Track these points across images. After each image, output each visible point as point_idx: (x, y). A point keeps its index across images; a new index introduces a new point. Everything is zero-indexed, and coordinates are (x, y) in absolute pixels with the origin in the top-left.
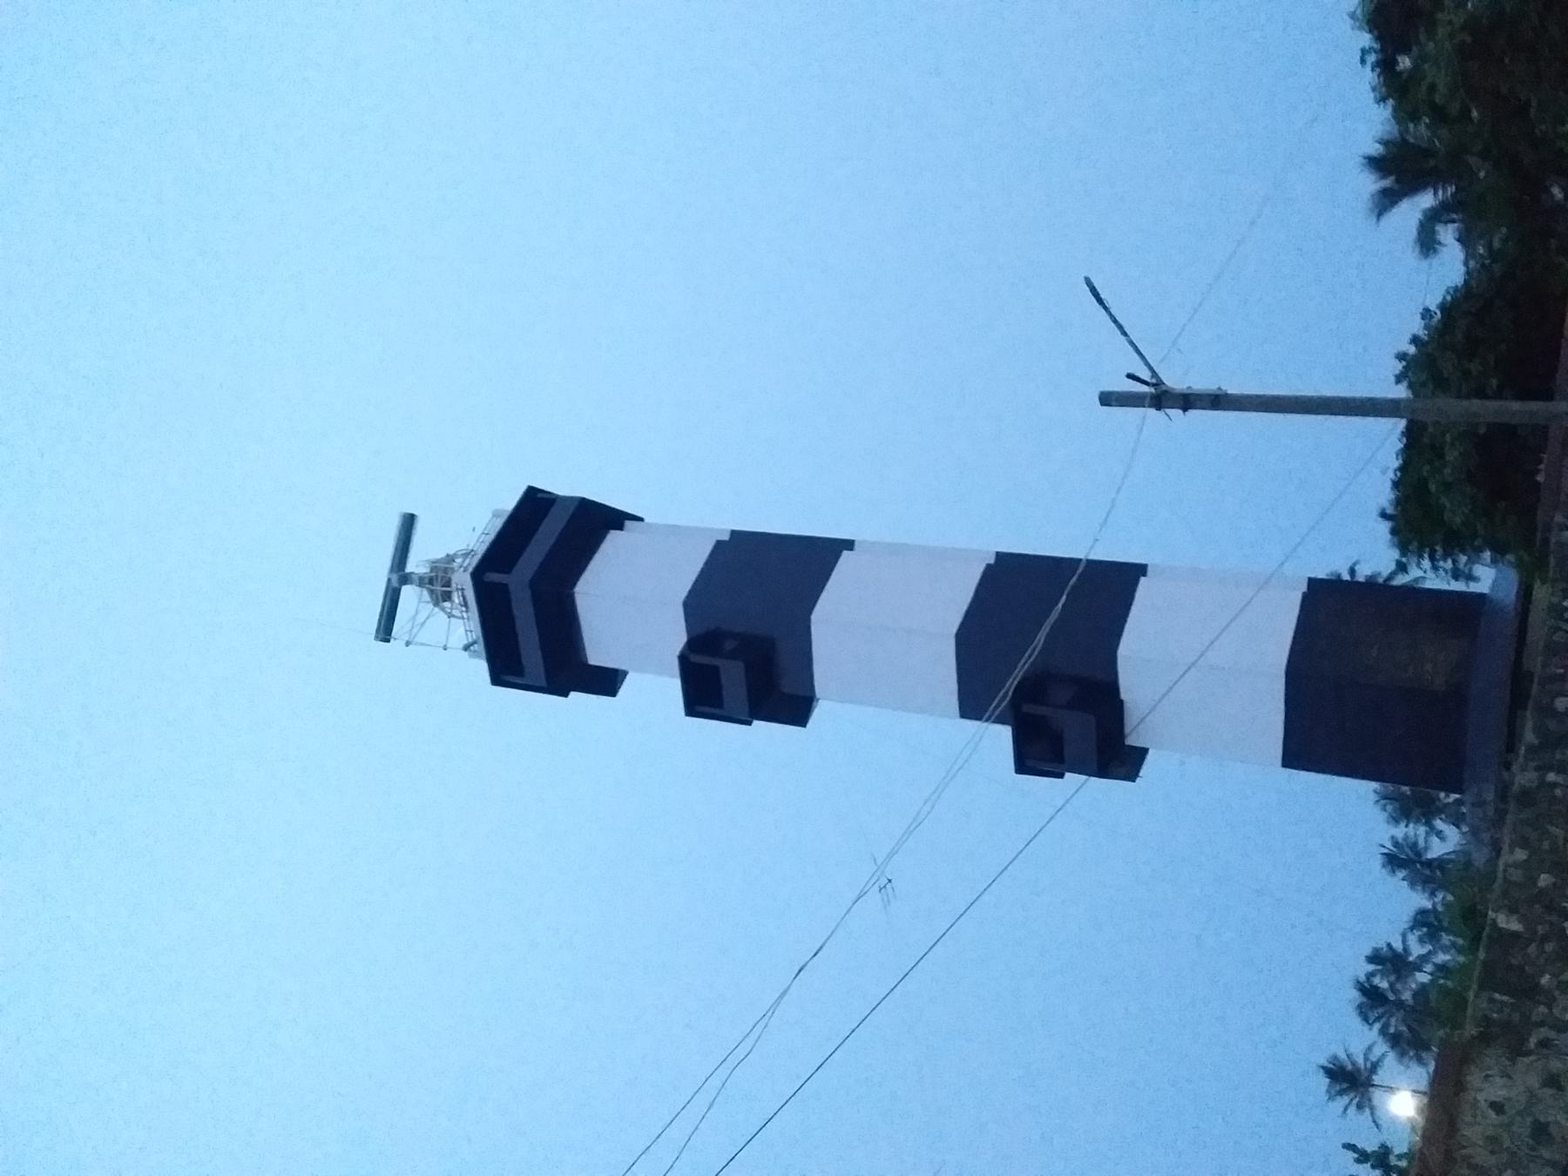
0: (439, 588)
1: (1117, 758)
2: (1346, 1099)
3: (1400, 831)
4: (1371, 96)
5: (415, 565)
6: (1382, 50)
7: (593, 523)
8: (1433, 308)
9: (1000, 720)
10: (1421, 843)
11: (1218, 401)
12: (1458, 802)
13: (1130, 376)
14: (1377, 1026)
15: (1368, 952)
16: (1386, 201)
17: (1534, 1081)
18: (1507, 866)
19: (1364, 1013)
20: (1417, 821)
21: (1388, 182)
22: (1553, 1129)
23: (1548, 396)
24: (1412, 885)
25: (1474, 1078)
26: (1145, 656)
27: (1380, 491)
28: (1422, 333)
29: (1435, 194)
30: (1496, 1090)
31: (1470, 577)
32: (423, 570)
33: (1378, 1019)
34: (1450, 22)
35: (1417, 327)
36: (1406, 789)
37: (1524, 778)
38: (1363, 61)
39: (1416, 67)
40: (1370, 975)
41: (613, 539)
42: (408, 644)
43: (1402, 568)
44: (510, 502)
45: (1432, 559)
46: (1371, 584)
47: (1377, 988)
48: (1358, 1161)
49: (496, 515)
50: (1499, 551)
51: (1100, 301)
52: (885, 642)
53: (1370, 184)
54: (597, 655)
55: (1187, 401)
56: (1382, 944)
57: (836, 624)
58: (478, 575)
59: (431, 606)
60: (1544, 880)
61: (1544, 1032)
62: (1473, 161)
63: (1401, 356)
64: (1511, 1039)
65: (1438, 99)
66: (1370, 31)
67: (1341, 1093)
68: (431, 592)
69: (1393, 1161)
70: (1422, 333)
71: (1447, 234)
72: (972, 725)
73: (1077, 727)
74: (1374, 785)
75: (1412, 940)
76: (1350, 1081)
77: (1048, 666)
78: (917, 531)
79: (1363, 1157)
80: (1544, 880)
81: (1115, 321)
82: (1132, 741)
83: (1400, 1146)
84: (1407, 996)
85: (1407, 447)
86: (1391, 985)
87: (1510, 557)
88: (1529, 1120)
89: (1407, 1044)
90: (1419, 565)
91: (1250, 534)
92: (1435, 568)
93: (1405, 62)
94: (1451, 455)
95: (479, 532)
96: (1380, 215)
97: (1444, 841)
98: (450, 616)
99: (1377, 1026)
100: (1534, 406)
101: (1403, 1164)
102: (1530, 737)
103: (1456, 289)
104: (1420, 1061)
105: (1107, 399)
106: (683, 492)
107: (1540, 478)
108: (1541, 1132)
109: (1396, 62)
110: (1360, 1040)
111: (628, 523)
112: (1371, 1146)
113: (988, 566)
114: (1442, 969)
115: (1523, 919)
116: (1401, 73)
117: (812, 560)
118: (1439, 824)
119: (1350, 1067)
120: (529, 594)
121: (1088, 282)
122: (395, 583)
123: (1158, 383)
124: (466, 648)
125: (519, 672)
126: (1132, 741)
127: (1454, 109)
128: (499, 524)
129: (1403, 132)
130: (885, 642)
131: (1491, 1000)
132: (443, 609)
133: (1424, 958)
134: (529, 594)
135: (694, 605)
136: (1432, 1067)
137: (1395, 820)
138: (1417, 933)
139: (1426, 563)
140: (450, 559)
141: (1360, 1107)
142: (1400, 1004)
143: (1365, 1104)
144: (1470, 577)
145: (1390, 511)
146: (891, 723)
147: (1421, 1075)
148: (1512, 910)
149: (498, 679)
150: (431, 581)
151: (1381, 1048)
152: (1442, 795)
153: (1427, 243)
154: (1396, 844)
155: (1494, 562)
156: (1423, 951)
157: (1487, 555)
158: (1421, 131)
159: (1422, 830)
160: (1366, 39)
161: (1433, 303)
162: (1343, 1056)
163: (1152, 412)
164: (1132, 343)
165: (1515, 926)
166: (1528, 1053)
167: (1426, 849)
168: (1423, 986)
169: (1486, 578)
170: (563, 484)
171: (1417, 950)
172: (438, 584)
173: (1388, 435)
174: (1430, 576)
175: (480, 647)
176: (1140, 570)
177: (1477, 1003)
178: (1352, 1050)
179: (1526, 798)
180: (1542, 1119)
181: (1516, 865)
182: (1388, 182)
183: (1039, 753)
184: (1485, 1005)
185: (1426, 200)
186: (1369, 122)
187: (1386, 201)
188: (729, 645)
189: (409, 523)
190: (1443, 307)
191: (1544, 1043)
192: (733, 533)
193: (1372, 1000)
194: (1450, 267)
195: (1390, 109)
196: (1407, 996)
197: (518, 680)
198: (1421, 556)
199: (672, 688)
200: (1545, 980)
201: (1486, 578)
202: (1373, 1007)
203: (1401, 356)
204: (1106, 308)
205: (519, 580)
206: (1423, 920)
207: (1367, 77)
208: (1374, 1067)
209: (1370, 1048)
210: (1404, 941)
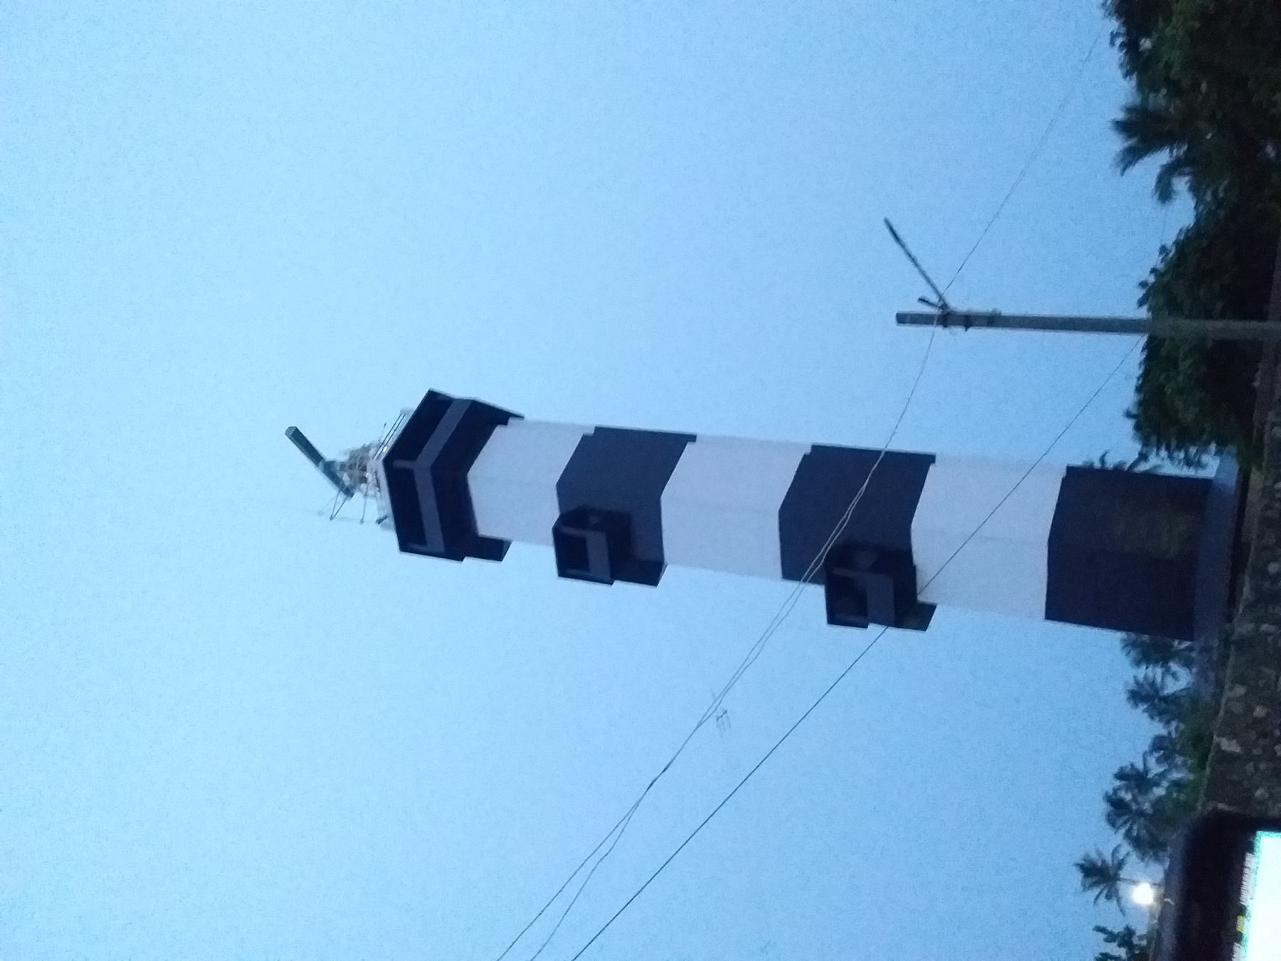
1: (910, 611)
2: (1096, 891)
3: (1142, 672)
4: (1118, 73)
6: (1128, 33)
7: (482, 421)
9: (814, 581)
10: (1159, 679)
11: (993, 320)
12: (1190, 649)
13: (922, 300)
14: (1123, 831)
15: (1116, 770)
16: (1131, 157)
19: (1112, 821)
20: (1156, 662)
23: (1262, 317)
24: (1152, 717)
26: (933, 529)
27: (1127, 396)
28: (1161, 266)
29: (1171, 151)
31: (1199, 465)
33: (1125, 823)
35: (1155, 260)
37: (1243, 628)
38: (1112, 43)
40: (1116, 791)
41: (499, 431)
42: (332, 518)
43: (1143, 457)
44: (414, 403)
45: (1168, 449)
46: (1118, 470)
48: (1106, 940)
49: (403, 413)
52: (721, 517)
53: (1117, 144)
54: (487, 527)
55: (968, 321)
56: (1126, 763)
57: (680, 502)
58: (388, 462)
60: (1259, 711)
62: (1202, 124)
63: (1143, 284)
65: (1173, 74)
70: (1161, 266)
71: (1181, 184)
72: (792, 585)
73: (878, 587)
75: (1152, 761)
76: (1101, 876)
77: (854, 537)
79: (1111, 937)
80: (1259, 711)
82: (921, 598)
84: (1147, 806)
86: (1134, 799)
87: (1233, 449)
89: (1147, 846)
92: (1171, 457)
93: (1146, 44)
94: (1184, 366)
96: (1124, 169)
97: (1178, 680)
101: (1144, 943)
102: (1247, 592)
104: (1157, 859)
105: (902, 319)
106: (555, 396)
107: (1256, 384)
110: (1108, 842)
111: (511, 421)
112: (1118, 928)
113: (805, 457)
114: (1177, 785)
115: (1242, 745)
116: (1143, 52)
117: (663, 451)
118: (1174, 666)
119: (1099, 864)
120: (430, 477)
121: (887, 223)
123: (944, 306)
126: (921, 598)
127: (1186, 83)
129: (1145, 99)
130: (721, 517)
133: (1162, 775)
134: (430, 477)
135: (565, 487)
137: (1137, 663)
138: (1157, 755)
140: (366, 449)
142: (1141, 813)
143: (1112, 894)
144: (1199, 465)
146: (726, 585)
150: (351, 467)
151: (1126, 848)
153: (1164, 192)
154: (1137, 682)
156: (1160, 769)
157: (1213, 447)
158: (1159, 100)
159: (1159, 671)
160: (1114, 25)
161: (1170, 238)
162: (1094, 855)
163: (939, 330)
167: (1163, 687)
169: (1212, 465)
170: (459, 388)
171: (1155, 769)
173: (1132, 349)
174: (1165, 464)
175: (390, 521)
176: (930, 459)
179: (1245, 644)
181: (1238, 699)
183: (846, 608)
185: (1162, 157)
186: (1115, 90)
187: (1131, 157)
188: (594, 520)
193: (1118, 809)
194: (1183, 211)
196: (1147, 806)
197: (416, 547)
198: (1158, 449)
199: (547, 555)
201: (1212, 465)
202: (1119, 816)
203: (1143, 284)
204: (903, 246)
206: (1159, 744)
207: (1113, 57)
208: (1120, 865)
209: (1116, 850)
210: (1145, 760)
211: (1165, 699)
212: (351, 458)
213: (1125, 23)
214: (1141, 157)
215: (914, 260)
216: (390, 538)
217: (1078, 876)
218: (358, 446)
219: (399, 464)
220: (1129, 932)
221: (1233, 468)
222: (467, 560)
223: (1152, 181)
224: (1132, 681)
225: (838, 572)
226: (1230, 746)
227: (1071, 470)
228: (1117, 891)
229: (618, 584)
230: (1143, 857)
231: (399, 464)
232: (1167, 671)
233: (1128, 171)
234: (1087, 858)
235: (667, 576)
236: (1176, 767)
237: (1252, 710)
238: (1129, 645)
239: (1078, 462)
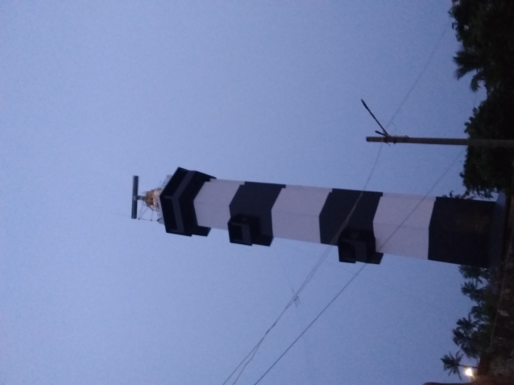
1: (374, 257)
2: (449, 370)
3: (467, 281)
5: (141, 192)
8: (477, 107)
9: (335, 245)
10: (475, 284)
11: (406, 140)
12: (487, 271)
13: (377, 132)
14: (460, 345)
16: (461, 73)
19: (456, 341)
24: (472, 298)
25: (492, 366)
26: (382, 222)
28: (473, 116)
33: (460, 343)
35: (471, 114)
36: (470, 267)
38: (453, 27)
40: (458, 329)
41: (206, 184)
43: (467, 193)
44: (172, 172)
45: (478, 191)
46: (457, 197)
49: (168, 176)
52: (296, 218)
53: (455, 67)
54: (201, 222)
55: (396, 140)
57: (279, 211)
58: (162, 197)
63: (466, 124)
67: (448, 367)
70: (473, 116)
71: (481, 84)
74: (459, 265)
75: (472, 317)
76: (452, 364)
77: (350, 225)
78: (307, 170)
84: (470, 335)
86: (465, 332)
89: (470, 351)
90: (473, 193)
92: (478, 194)
93: (467, 27)
97: (483, 283)
98: (153, 210)
104: (474, 357)
105: (369, 139)
106: (229, 168)
110: (454, 350)
111: (211, 179)
114: (482, 326)
117: (273, 191)
118: (481, 278)
119: (451, 359)
120: (179, 203)
123: (386, 134)
124: (158, 220)
128: (168, 181)
132: (150, 208)
133: (476, 323)
134: (179, 203)
135: (233, 206)
136: (479, 359)
137: (466, 277)
139: (476, 192)
140: (153, 191)
141: (455, 372)
142: (468, 338)
145: (463, 174)
146: (296, 251)
147: (475, 361)
149: (168, 230)
151: (462, 352)
153: (474, 86)
154: (465, 283)
155: (498, 192)
158: (472, 50)
159: (475, 280)
160: (454, 20)
162: (449, 356)
167: (477, 286)
168: (475, 332)
171: (473, 320)
172: (148, 199)
174: (477, 196)
175: (162, 220)
176: (380, 194)
182: (461, 67)
183: (347, 255)
186: (454, 46)
187: (461, 73)
190: (480, 108)
193: (458, 337)
194: (482, 94)
195: (462, 42)
196: (470, 335)
199: (226, 233)
203: (466, 124)
205: (175, 199)
206: (475, 310)
208: (459, 359)
210: (469, 316)
211: (477, 291)
216: (162, 227)
217: (442, 364)
218: (149, 190)
219: (167, 197)
222: (194, 236)
224: (464, 285)
226: (504, 314)
227: (438, 198)
229: (254, 246)
231: (167, 197)
233: (441, 361)
235: (275, 241)
238: (462, 270)
239: (440, 195)
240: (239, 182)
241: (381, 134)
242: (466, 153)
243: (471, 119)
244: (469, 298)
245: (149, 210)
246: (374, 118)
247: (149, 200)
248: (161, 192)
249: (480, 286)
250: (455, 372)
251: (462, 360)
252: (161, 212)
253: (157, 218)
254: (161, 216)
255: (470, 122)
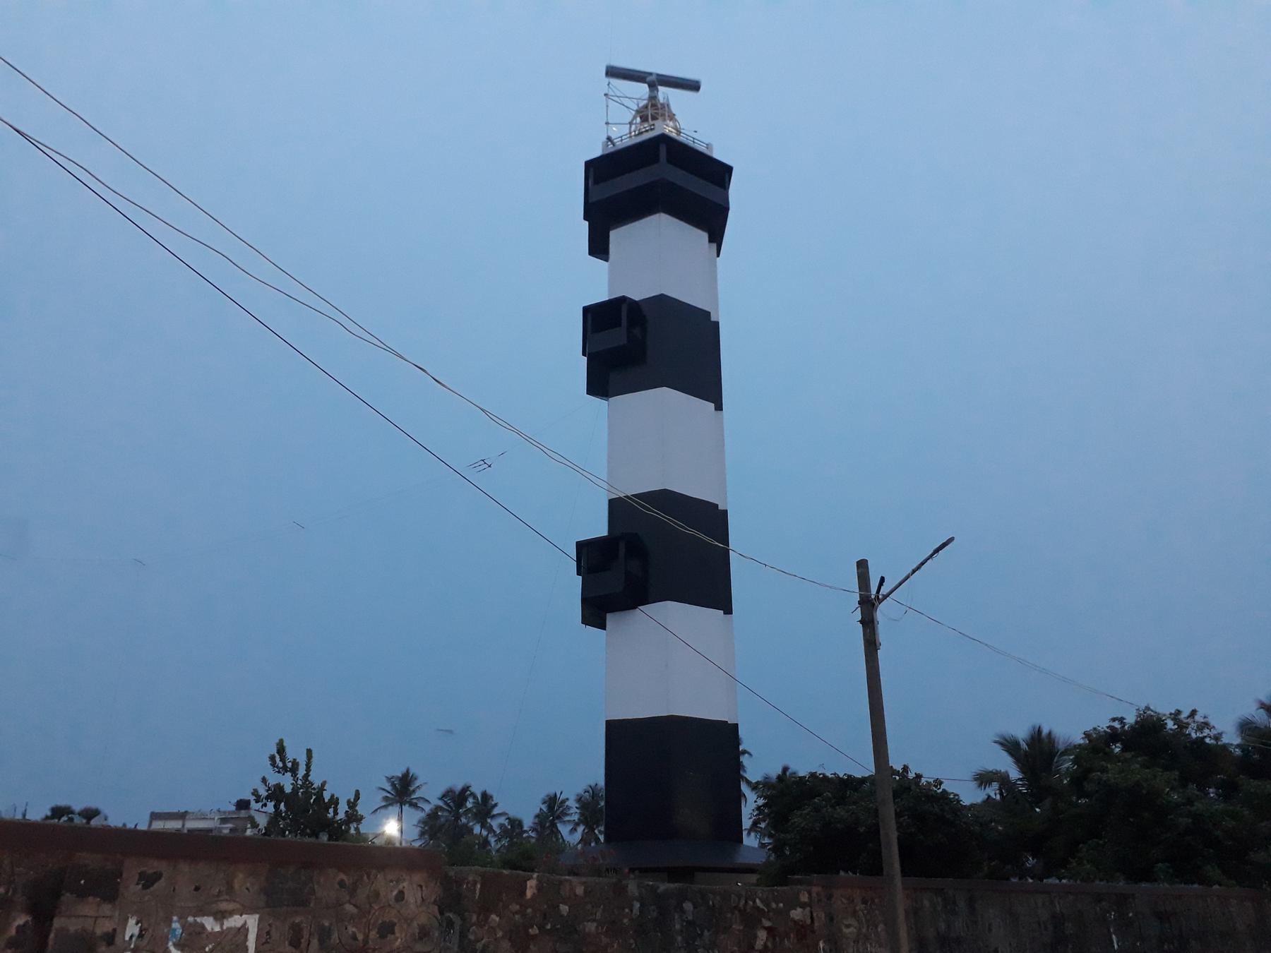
0: (650, 112)
1: (596, 611)
2: (389, 788)
3: (572, 803)
4: (1089, 728)
5: (663, 91)
6: (1124, 732)
7: (711, 219)
10: (567, 818)
11: (871, 645)
12: (597, 840)
13: (882, 580)
14: (441, 803)
15: (489, 792)
16: (1010, 746)
17: (423, 919)
18: (570, 881)
19: (448, 794)
20: (582, 814)
21: (1024, 746)
22: (390, 937)
23: (904, 873)
24: (537, 816)
25: (418, 877)
30: (412, 897)
32: (661, 98)
33: (446, 803)
34: (1155, 777)
37: (632, 887)
38: (1114, 720)
39: (1117, 758)
40: (473, 795)
41: (705, 236)
44: (718, 155)
45: (764, 805)
46: (739, 766)
47: (466, 800)
48: (349, 802)
49: (708, 146)
50: (777, 849)
51: (937, 551)
52: (655, 440)
53: (1021, 733)
54: (617, 237)
55: (868, 623)
57: (663, 403)
58: (664, 138)
59: (635, 108)
60: (564, 909)
61: (458, 922)
62: (1048, 802)
64: (450, 900)
65: (1095, 775)
66: (1137, 722)
67: (393, 785)
68: (646, 107)
69: (353, 826)
71: (993, 791)
74: (602, 783)
75: (502, 820)
76: (402, 791)
77: (653, 555)
78: (739, 452)
79: (352, 805)
80: (564, 909)
81: (922, 564)
82: (609, 617)
83: (363, 829)
84: (464, 820)
85: (841, 780)
86: (469, 810)
88: (396, 920)
89: (431, 825)
91: (771, 681)
92: (758, 808)
93: (1117, 749)
94: (840, 812)
95: (695, 135)
96: (1001, 744)
97: (570, 834)
98: (631, 123)
99: (441, 803)
100: (897, 866)
101: (352, 831)
102: (663, 887)
103: (959, 801)
104: (422, 834)
105: (862, 565)
106: (742, 282)
107: (842, 873)
108: (387, 930)
109: (1115, 742)
110: (431, 791)
111: (714, 246)
112: (360, 809)
114: (486, 842)
116: (1109, 746)
117: (704, 381)
118: (581, 829)
120: (656, 181)
121: (951, 540)
122: (649, 79)
124: (609, 139)
125: (596, 182)
126: (609, 617)
128: (702, 149)
131: (475, 883)
132: (635, 118)
133: (490, 830)
134: (656, 181)
135: (662, 302)
137: (579, 800)
138: (506, 823)
139: (761, 802)
140: (672, 117)
141: (386, 798)
142: (458, 817)
143: (388, 802)
146: (599, 453)
148: (540, 888)
149: (589, 165)
151: (428, 808)
152: (602, 828)
153: (984, 779)
154: (564, 802)
155: (762, 846)
156: (495, 828)
159: (576, 817)
160: (1131, 719)
162: (417, 783)
164: (908, 577)
165: (529, 894)
166: (441, 913)
172: (652, 111)
173: (862, 765)
174: (751, 803)
175: (611, 148)
176: (728, 610)
177: (472, 874)
178: (423, 788)
179: (620, 890)
180: (397, 929)
181: (572, 889)
183: (591, 556)
184: (471, 878)
185: (1014, 774)
186: (1070, 728)
187: (1010, 746)
189: (693, 86)
191: (450, 924)
192: (717, 324)
193: (457, 798)
194: (970, 795)
196: (464, 820)
199: (601, 294)
200: (494, 918)
202: (453, 800)
205: (664, 171)
206: (516, 824)
208: (414, 805)
211: (553, 825)
212: (663, 105)
213: (1131, 726)
214: (1012, 755)
215: (918, 568)
216: (596, 151)
218: (674, 109)
219: (663, 151)
220: (359, 819)
221: (759, 858)
222: (586, 225)
223: (991, 767)
225: (622, 547)
228: (391, 804)
229: (584, 360)
230: (424, 822)
231: (663, 151)
232: (577, 824)
233: (998, 747)
234: (414, 778)
236: (499, 840)
237: (565, 904)
238: (593, 790)
239: (742, 732)
240: (717, 310)
241: (878, 591)
242: (829, 774)
243: (919, 776)
244: (537, 811)
245: (629, 116)
246: (914, 571)
247: (650, 112)
248: (674, 135)
249: (564, 829)
250: (386, 798)
251: (412, 810)
252: (628, 142)
253: (615, 132)
254: (620, 145)
255: (911, 775)
